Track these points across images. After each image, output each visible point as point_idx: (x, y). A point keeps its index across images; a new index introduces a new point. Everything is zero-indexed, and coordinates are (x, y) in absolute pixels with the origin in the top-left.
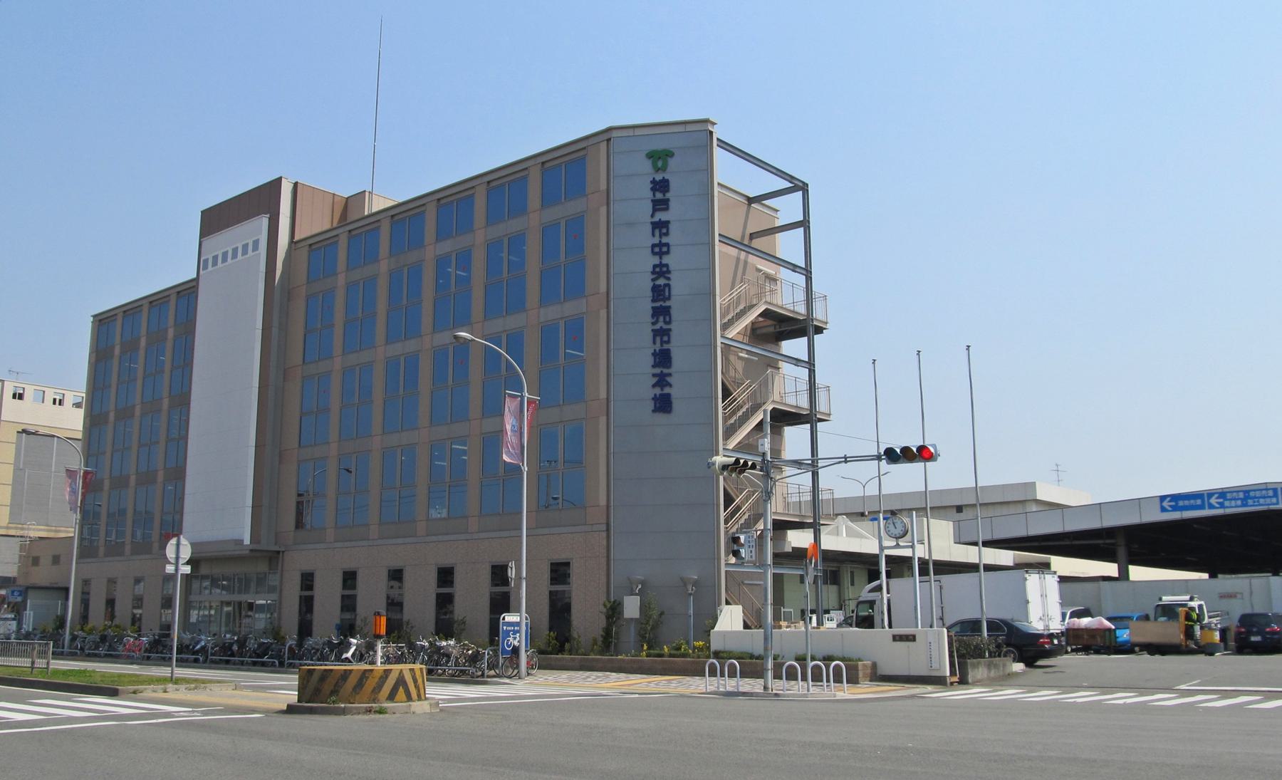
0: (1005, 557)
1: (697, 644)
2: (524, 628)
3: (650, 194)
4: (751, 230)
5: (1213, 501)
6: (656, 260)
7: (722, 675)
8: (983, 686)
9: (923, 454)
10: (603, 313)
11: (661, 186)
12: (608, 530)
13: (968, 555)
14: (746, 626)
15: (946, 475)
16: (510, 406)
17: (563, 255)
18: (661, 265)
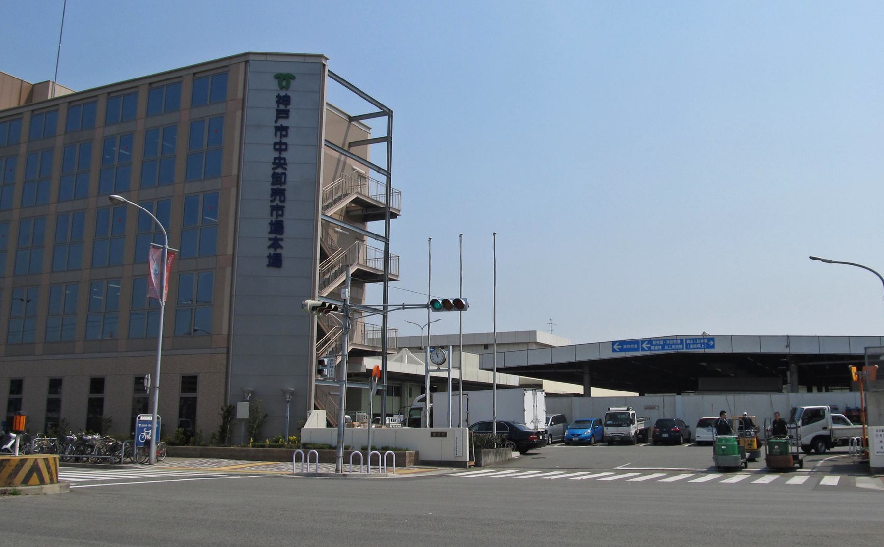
0: (514, 380)
1: (291, 438)
2: (156, 426)
3: (276, 106)
4: (350, 139)
5: (644, 346)
6: (277, 155)
7: (306, 461)
10: (234, 190)
11: (284, 100)
12: (228, 353)
13: (486, 377)
14: (329, 425)
15: (475, 322)
16: (153, 256)
18: (280, 159)
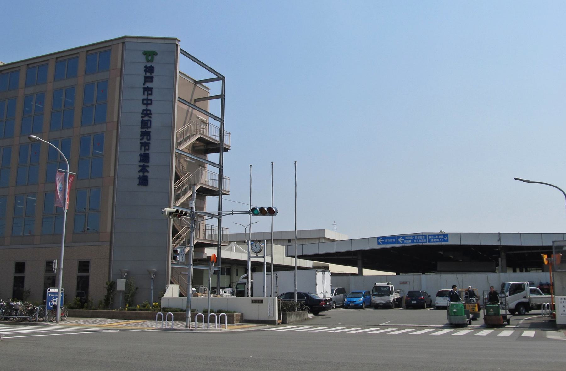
0: (309, 264)
1: (154, 304)
3: (144, 73)
4: (195, 97)
5: (400, 240)
6: (144, 107)
7: (165, 320)
8: (293, 325)
9: (271, 212)
10: (115, 132)
11: (149, 69)
12: (111, 245)
13: (290, 262)
14: (181, 295)
15: (282, 224)
17: (95, 99)
18: (147, 110)
